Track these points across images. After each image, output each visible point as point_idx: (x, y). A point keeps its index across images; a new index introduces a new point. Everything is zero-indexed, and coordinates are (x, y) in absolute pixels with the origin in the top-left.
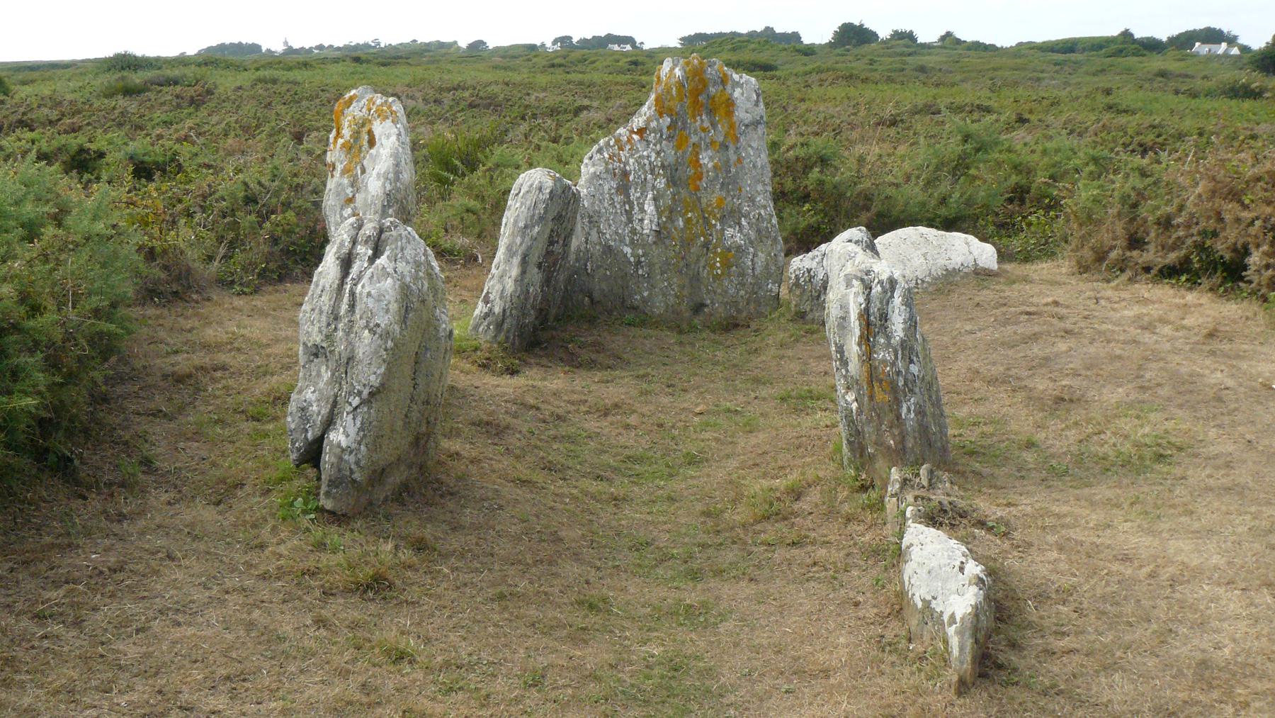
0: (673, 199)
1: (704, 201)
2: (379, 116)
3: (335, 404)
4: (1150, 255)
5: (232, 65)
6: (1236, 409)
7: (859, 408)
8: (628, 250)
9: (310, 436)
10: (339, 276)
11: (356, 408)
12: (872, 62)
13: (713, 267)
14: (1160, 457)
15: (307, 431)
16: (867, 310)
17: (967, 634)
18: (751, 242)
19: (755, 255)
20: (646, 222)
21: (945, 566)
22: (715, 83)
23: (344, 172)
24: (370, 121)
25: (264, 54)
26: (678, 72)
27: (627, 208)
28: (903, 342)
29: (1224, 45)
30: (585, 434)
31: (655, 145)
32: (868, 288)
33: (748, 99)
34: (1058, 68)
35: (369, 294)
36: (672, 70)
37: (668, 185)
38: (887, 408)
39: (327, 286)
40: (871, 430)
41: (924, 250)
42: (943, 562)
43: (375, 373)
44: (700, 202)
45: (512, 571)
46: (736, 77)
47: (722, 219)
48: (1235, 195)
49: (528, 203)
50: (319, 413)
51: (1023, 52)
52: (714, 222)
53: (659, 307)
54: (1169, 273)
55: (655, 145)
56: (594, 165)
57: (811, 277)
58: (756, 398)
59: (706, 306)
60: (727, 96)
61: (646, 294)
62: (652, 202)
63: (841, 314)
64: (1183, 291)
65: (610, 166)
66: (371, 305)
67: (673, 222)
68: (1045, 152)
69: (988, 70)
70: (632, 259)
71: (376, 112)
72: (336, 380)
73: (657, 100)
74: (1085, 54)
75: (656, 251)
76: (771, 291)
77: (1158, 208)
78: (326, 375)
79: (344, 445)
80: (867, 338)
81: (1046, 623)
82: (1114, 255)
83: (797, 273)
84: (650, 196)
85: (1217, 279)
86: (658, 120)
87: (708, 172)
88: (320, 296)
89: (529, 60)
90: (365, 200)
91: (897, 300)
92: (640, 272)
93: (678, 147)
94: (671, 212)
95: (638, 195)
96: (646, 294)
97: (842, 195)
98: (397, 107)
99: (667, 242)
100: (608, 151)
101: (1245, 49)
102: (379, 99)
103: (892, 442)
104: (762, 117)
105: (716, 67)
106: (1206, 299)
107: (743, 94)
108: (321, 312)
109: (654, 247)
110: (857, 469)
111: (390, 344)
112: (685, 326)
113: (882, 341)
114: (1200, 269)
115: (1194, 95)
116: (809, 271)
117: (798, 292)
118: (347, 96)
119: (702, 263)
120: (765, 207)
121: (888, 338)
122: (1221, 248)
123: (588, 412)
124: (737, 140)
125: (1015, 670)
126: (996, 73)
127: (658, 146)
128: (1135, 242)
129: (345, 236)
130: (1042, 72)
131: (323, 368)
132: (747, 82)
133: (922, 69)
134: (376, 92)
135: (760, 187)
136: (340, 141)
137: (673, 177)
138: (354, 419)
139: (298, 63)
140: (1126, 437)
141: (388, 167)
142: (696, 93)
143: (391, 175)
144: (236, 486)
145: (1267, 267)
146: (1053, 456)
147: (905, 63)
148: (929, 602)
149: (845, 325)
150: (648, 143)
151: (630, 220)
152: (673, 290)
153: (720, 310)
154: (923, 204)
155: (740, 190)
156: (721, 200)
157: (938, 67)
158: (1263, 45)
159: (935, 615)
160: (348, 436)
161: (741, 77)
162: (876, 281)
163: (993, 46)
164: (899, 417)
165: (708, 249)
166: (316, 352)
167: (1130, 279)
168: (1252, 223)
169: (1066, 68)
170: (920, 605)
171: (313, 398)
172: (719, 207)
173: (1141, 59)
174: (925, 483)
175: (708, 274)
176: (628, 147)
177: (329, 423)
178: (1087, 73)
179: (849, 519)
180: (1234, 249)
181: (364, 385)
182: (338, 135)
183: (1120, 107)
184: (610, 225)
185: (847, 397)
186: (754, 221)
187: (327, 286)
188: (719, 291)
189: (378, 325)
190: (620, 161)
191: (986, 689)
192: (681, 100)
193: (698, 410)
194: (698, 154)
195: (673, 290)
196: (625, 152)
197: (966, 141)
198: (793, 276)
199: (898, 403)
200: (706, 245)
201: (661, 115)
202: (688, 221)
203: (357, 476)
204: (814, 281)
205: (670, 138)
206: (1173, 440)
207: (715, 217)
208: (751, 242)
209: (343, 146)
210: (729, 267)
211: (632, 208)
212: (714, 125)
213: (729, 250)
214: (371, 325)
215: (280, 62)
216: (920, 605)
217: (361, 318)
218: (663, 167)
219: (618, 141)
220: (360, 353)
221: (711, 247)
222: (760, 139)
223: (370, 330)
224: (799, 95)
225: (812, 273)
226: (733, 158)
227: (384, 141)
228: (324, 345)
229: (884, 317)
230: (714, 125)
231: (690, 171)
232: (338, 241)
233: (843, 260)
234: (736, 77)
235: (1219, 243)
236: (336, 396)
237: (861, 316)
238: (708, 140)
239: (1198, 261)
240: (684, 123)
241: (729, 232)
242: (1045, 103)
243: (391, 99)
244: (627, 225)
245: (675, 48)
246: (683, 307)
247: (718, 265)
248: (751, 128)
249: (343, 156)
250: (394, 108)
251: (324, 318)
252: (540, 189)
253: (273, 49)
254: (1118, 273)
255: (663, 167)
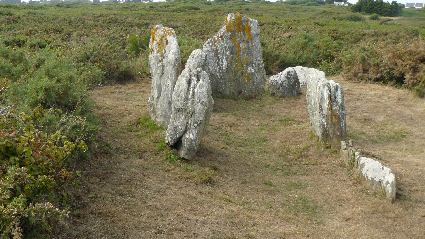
0: (232, 58)
1: (241, 59)
2: (168, 34)
3: (187, 126)
4: (371, 75)
5: (16, 7)
6: (418, 122)
7: (327, 124)
8: (218, 74)
9: (178, 136)
10: (187, 86)
11: (195, 127)
12: (231, 7)
13: (245, 79)
14: (403, 136)
15: (177, 135)
16: (330, 95)
17: (395, 186)
18: (256, 72)
19: (257, 76)
20: (224, 65)
21: (378, 168)
22: (245, 22)
23: (158, 52)
24: (165, 36)
25: (22, 3)
26: (233, 18)
27: (218, 61)
28: (341, 104)
29: (343, 3)
30: (229, 133)
31: (226, 41)
32: (330, 89)
33: (255, 27)
34: (291, 9)
35: (200, 92)
36: (231, 17)
37: (230, 54)
38: (337, 124)
39: (183, 90)
40: (332, 130)
41: (304, 74)
42: (377, 167)
43: (202, 116)
44: (240, 59)
45: (242, 175)
46: (251, 20)
47: (247, 65)
48: (400, 57)
49: (198, 60)
50: (181, 129)
51: (279, 4)
52: (245, 65)
53: (227, 92)
54: (377, 80)
55: (226, 41)
56: (207, 47)
57: (277, 83)
58: (272, 120)
59: (242, 92)
60: (248, 26)
61: (224, 88)
62: (225, 59)
63: (321, 96)
64: (384, 86)
65: (212, 48)
66: (201, 96)
67: (232, 65)
68: (323, 41)
69: (269, 10)
70: (219, 77)
71: (167, 33)
72: (187, 118)
73: (226, 27)
74: (299, 5)
75: (226, 75)
76: (262, 87)
77: (374, 61)
78: (183, 117)
79: (192, 138)
80: (330, 103)
81: (406, 183)
82: (360, 75)
83: (272, 81)
84: (225, 57)
85: (393, 82)
86: (227, 33)
87: (242, 50)
88: (181, 93)
89: (115, 6)
90: (167, 61)
91: (339, 92)
92: (222, 81)
93: (233, 42)
94: (231, 62)
95: (221, 57)
96: (224, 88)
97: (270, 56)
98: (173, 31)
99: (230, 72)
100: (211, 43)
101: (349, 4)
102: (167, 29)
103: (338, 133)
104: (259, 33)
105: (245, 16)
106: (391, 88)
107: (253, 25)
108: (181, 98)
109: (226, 73)
110: (325, 142)
111: (206, 107)
112: (236, 98)
113: (335, 104)
114: (387, 79)
115: (340, 19)
116: (276, 81)
117: (272, 87)
118: (155, 27)
119: (241, 79)
120: (260, 61)
121: (337, 103)
122: (396, 73)
123: (226, 126)
124: (252, 40)
125: (405, 196)
126: (272, 11)
127: (227, 42)
128: (365, 71)
129: (187, 74)
130: (286, 11)
131: (181, 115)
132: (255, 22)
133: (247, 10)
134: (165, 26)
135: (259, 55)
136: (155, 42)
137: (231, 51)
138: (195, 131)
139: (39, 7)
140: (391, 130)
141: (176, 51)
142: (239, 25)
143: (177, 53)
144: (144, 153)
145: (411, 79)
146: (370, 136)
147: (241, 7)
148: (374, 179)
149: (323, 99)
150: (224, 40)
151: (219, 65)
152: (232, 87)
153: (247, 93)
154: (294, 59)
155: (253, 55)
156: (247, 59)
157: (252, 9)
158: (356, 3)
159: (376, 182)
160: (193, 136)
161: (253, 20)
162: (332, 86)
163: (270, 2)
164: (340, 126)
165: (243, 74)
166: (179, 110)
167: (365, 82)
168: (406, 66)
169: (294, 9)
170: (371, 179)
171: (179, 124)
172: (246, 61)
173: (317, 7)
174: (351, 145)
175: (243, 82)
176: (218, 42)
177: (185, 132)
178: (301, 11)
179: (327, 156)
180: (400, 73)
181: (199, 120)
182: (153, 39)
183: (319, 24)
184: (212, 67)
185: (323, 121)
186: (257, 65)
187: (183, 90)
188: (246, 87)
189: (203, 102)
190: (215, 46)
191: (400, 202)
192: (234, 27)
193: (257, 124)
194: (239, 44)
195: (232, 87)
196: (217, 43)
197: (306, 39)
198: (271, 82)
199: (340, 122)
200: (242, 73)
201: (228, 32)
202: (236, 65)
203: (195, 148)
204: (278, 84)
205: (231, 39)
206: (405, 131)
207: (245, 64)
208: (256, 72)
209: (157, 44)
210: (249, 80)
211: (219, 61)
212: (244, 35)
213: (249, 74)
214: (201, 102)
215: (33, 6)
216: (371, 179)
217: (197, 100)
218: (229, 48)
219: (214, 40)
220: (197, 110)
221: (244, 73)
222: (259, 39)
223: (201, 103)
224: (213, 19)
225: (277, 81)
226: (250, 45)
227: (172, 42)
228: (182, 108)
229: (335, 97)
230: (244, 35)
231: (237, 50)
232: (186, 76)
233: (318, 80)
234: (251, 20)
235: (395, 72)
236: (187, 123)
237: (329, 97)
238: (243, 40)
239: (387, 77)
240: (235, 34)
241: (249, 69)
242: (295, 22)
243: (171, 29)
244: (217, 66)
245: (164, 2)
246: (235, 92)
247: (246, 79)
248: (256, 36)
249: (157, 47)
250: (173, 32)
251: (183, 100)
252: (202, 56)
253: (25, 2)
254: (361, 80)
255: (229, 48)
